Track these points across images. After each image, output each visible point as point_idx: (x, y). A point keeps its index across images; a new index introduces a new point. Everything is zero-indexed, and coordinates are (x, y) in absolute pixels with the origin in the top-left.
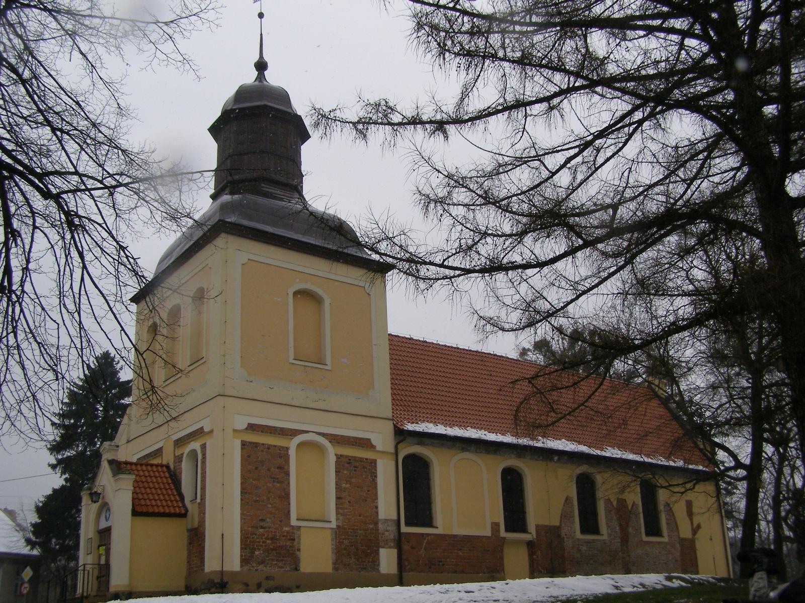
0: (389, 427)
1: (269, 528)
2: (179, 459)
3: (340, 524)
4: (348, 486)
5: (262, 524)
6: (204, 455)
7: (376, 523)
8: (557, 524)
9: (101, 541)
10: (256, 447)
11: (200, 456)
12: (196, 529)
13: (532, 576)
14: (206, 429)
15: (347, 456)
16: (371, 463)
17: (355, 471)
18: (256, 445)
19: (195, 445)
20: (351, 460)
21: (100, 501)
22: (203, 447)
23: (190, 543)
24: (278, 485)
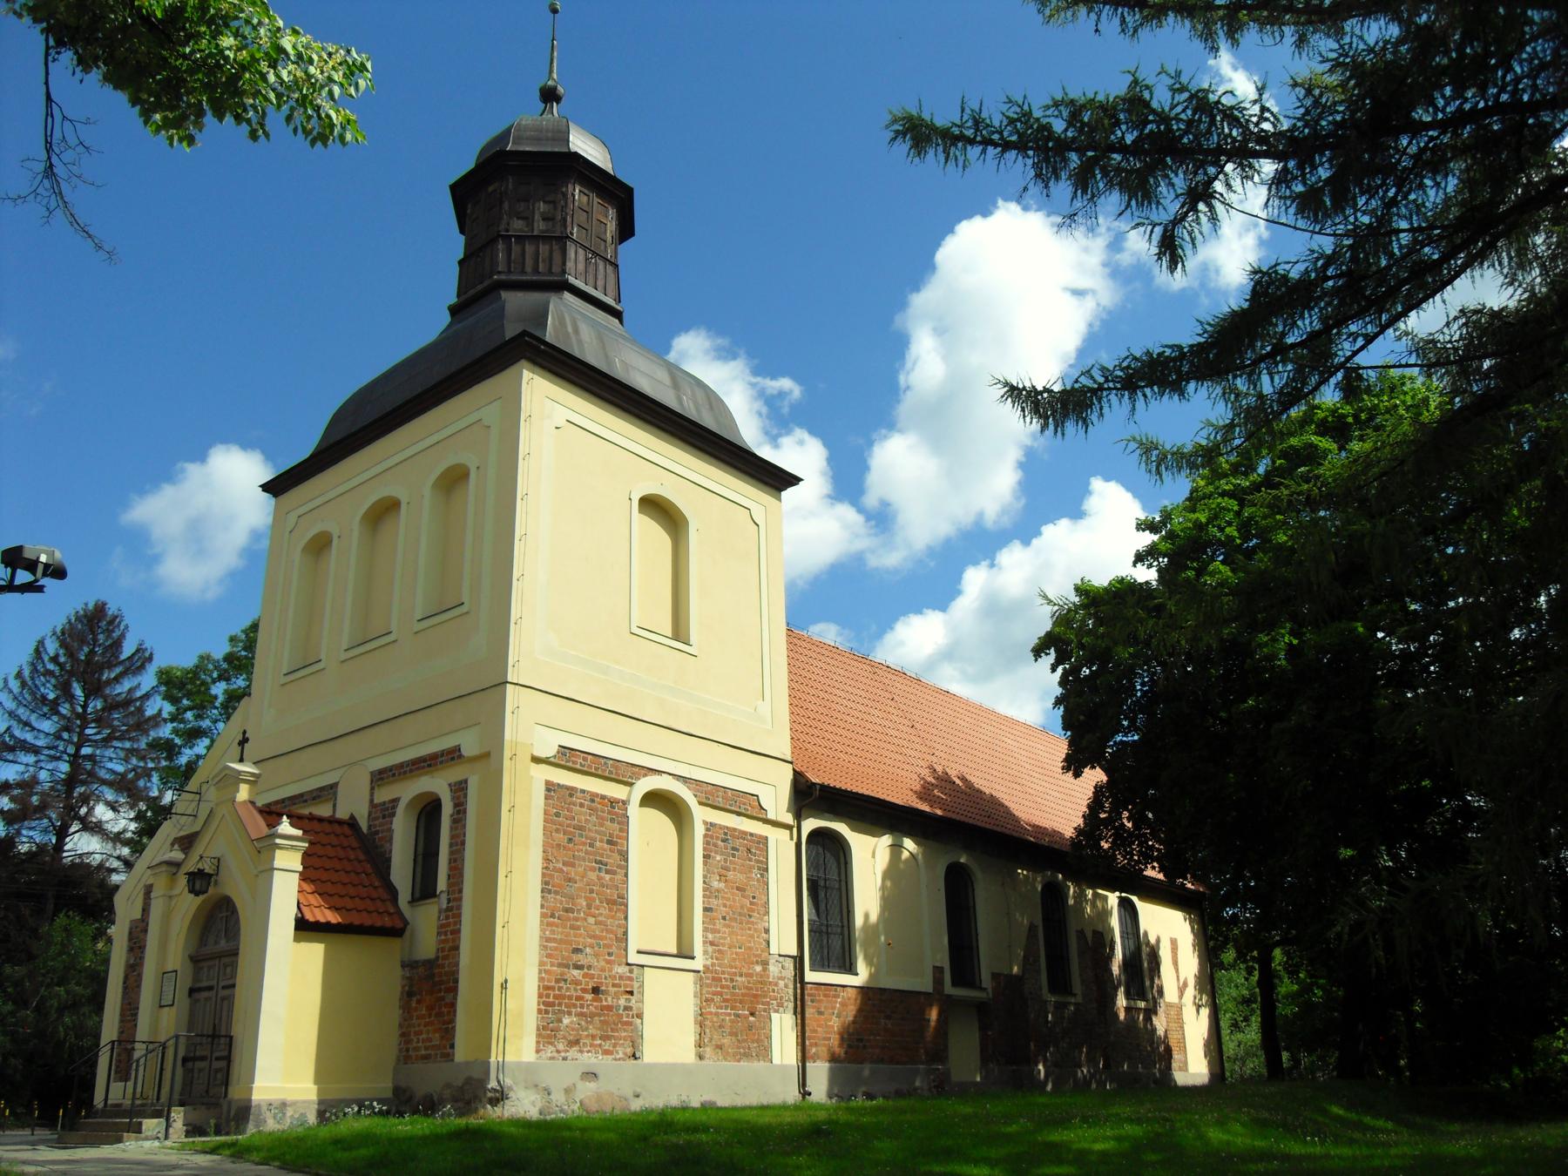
0: (786, 776)
1: (589, 967)
2: (385, 811)
4: (722, 885)
5: (575, 957)
7: (765, 963)
9: (196, 978)
10: (571, 795)
12: (430, 964)
14: (466, 752)
15: (721, 827)
18: (572, 791)
19: (437, 784)
20: (729, 834)
21: (211, 890)
22: (460, 789)
23: (410, 994)
24: (608, 877)
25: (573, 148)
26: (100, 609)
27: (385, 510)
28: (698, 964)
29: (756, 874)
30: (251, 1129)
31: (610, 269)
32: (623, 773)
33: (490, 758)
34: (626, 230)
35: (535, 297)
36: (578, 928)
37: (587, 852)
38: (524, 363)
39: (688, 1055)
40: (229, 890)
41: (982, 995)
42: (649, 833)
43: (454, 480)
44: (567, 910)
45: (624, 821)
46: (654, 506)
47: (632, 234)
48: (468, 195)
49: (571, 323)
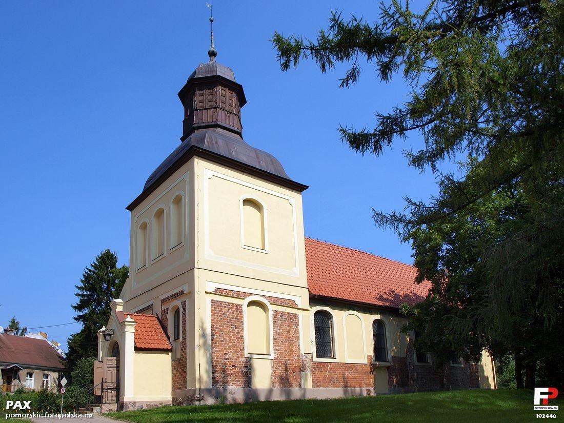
1: (231, 359)
2: (165, 312)
3: (276, 356)
4: (281, 331)
6: (184, 309)
7: (299, 356)
8: (405, 356)
11: (181, 311)
13: (172, 398)
16: (295, 316)
17: (285, 321)
19: (177, 303)
20: (282, 314)
22: (184, 303)
23: (175, 369)
25: (218, 73)
26: (108, 252)
27: (160, 214)
28: (272, 357)
29: (294, 327)
30: (124, 410)
31: (235, 117)
32: (240, 295)
33: (191, 293)
34: (242, 101)
35: (201, 131)
36: (226, 347)
37: (228, 322)
38: (195, 156)
39: (311, 388)
40: (116, 339)
41: (388, 364)
42: (251, 315)
43: (178, 200)
44: (221, 341)
45: (241, 312)
46: (248, 202)
47: (245, 102)
48: (186, 95)
49: (215, 140)
